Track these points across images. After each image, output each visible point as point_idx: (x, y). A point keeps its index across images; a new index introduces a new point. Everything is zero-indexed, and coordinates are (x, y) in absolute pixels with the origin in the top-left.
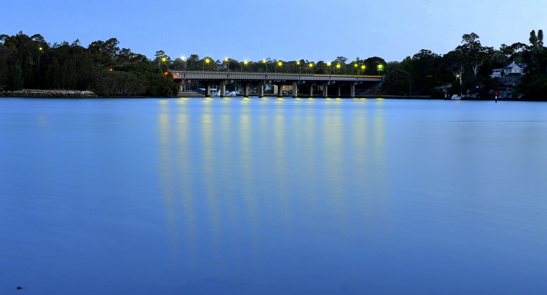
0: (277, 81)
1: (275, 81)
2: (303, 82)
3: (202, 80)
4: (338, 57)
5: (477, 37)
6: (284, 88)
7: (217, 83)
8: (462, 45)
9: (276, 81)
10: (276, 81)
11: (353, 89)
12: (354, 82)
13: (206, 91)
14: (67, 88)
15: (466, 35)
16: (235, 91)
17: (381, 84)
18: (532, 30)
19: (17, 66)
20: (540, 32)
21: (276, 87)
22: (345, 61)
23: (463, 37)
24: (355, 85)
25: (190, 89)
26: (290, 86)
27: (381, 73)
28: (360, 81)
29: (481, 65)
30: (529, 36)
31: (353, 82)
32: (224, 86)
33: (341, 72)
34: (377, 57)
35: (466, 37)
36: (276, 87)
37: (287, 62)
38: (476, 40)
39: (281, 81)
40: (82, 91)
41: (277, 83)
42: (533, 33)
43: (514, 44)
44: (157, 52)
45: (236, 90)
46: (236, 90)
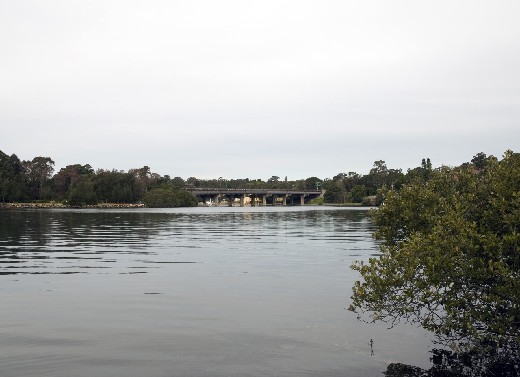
2: (307, 195)
3: (226, 195)
4: (273, 176)
5: (384, 162)
7: (212, 197)
8: (374, 168)
11: (15, 208)
12: (303, 194)
14: (116, 202)
15: (376, 161)
19: (99, 188)
20: (428, 160)
22: (278, 179)
23: (375, 163)
29: (396, 182)
30: (421, 162)
34: (14, 157)
35: (377, 163)
38: (384, 164)
42: (424, 160)
43: (417, 167)
45: (210, 201)
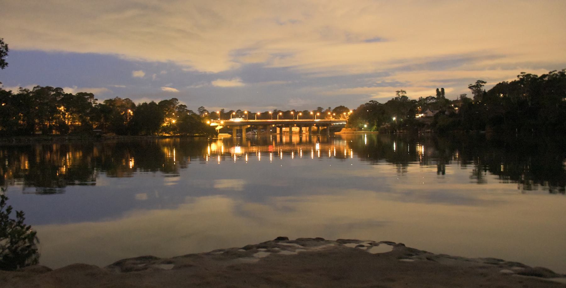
1: (277, 125)
44: (199, 108)
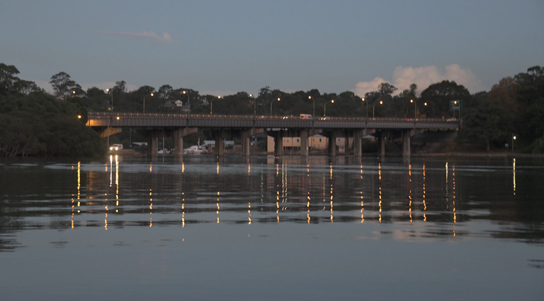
0: (274, 129)
6: (288, 141)
9: (271, 130)
10: (271, 130)
13: (148, 149)
16: (197, 145)
17: (455, 135)
18: (314, 88)
21: (271, 141)
24: (412, 135)
25: (401, 156)
26: (295, 139)
27: (457, 114)
28: (420, 129)
31: (406, 131)
32: (181, 140)
33: (379, 113)
36: (271, 141)
37: (322, 93)
39: (279, 129)
40: (24, 218)
41: (272, 134)
44: (54, 77)
46: (199, 143)
